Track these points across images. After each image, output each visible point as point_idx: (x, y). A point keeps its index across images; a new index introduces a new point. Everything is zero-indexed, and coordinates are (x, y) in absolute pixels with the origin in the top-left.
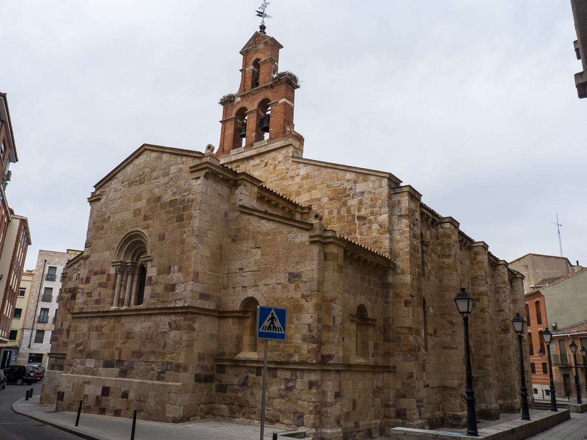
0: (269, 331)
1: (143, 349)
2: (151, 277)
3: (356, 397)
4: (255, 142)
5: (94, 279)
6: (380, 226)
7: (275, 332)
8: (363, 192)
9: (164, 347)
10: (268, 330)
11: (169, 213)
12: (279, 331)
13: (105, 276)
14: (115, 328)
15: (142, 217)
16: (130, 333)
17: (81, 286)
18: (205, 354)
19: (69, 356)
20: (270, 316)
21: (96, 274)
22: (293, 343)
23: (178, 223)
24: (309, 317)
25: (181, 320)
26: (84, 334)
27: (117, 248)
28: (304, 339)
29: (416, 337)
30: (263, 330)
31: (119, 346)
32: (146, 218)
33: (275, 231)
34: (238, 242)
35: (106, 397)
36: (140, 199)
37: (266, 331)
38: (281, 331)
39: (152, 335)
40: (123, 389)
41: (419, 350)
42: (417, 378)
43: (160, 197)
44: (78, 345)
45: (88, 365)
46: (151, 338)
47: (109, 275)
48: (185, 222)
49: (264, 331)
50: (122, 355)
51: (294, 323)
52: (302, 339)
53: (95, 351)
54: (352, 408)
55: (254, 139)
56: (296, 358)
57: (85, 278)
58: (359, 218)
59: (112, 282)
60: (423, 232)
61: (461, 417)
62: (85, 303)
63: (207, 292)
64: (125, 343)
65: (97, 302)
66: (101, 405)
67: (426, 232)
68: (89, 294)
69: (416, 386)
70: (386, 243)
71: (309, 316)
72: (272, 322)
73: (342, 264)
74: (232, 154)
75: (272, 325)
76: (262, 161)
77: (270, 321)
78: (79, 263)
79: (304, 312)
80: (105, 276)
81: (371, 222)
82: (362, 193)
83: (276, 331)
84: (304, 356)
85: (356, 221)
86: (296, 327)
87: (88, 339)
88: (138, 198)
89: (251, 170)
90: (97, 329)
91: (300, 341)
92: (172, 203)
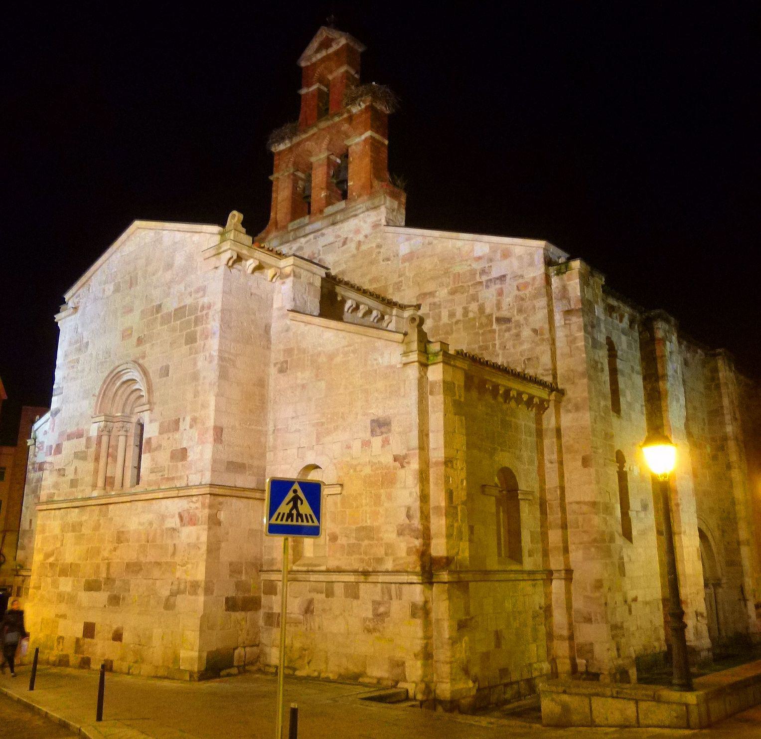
0: (289, 522)
1: (142, 559)
2: (150, 438)
3: (502, 627)
4: (326, 207)
5: (69, 447)
6: (535, 331)
7: (300, 523)
8: (504, 276)
9: (174, 554)
10: (287, 520)
11: (174, 330)
12: (308, 521)
13: (83, 440)
14: (100, 525)
15: (134, 339)
16: (123, 532)
17: (49, 459)
18: (241, 563)
19: (35, 574)
20: (291, 495)
21: (70, 437)
22: (382, 539)
23: (189, 346)
24: (408, 495)
25: (197, 508)
26: (55, 537)
27: (99, 394)
28: (400, 533)
29: (605, 519)
30: (277, 520)
31: (106, 554)
32: (140, 341)
33: (346, 349)
34: (288, 371)
35: (89, 640)
36: (131, 310)
37: (284, 522)
38: (313, 522)
39: (155, 534)
40: (115, 627)
41: (612, 540)
42: (609, 589)
43: (160, 306)
44: (47, 556)
45: (62, 588)
46: (154, 541)
47: (89, 439)
48: (200, 342)
49: (279, 522)
50: (112, 570)
51: (383, 505)
52: (398, 531)
53: (71, 564)
54: (493, 644)
55: (324, 202)
56: (389, 565)
57: (54, 446)
58: (499, 320)
59: (93, 449)
60: (614, 339)
61: (697, 649)
62: (56, 485)
63: (239, 460)
64: (115, 549)
65: (74, 483)
66: (82, 653)
67: (620, 337)
68: (61, 472)
69: (609, 601)
70: (546, 359)
71: (406, 493)
72: (295, 506)
73: (462, 399)
74: (290, 228)
75: (294, 512)
76: (339, 236)
77: (291, 504)
78: (555, 452)
79: (398, 485)
80: (83, 440)
81: (518, 325)
82: (502, 278)
83: (302, 521)
84: (401, 562)
85: (495, 326)
86: (387, 510)
87: (62, 545)
88: (129, 310)
89: (321, 253)
90: (76, 527)
91: (394, 536)
92: (180, 312)
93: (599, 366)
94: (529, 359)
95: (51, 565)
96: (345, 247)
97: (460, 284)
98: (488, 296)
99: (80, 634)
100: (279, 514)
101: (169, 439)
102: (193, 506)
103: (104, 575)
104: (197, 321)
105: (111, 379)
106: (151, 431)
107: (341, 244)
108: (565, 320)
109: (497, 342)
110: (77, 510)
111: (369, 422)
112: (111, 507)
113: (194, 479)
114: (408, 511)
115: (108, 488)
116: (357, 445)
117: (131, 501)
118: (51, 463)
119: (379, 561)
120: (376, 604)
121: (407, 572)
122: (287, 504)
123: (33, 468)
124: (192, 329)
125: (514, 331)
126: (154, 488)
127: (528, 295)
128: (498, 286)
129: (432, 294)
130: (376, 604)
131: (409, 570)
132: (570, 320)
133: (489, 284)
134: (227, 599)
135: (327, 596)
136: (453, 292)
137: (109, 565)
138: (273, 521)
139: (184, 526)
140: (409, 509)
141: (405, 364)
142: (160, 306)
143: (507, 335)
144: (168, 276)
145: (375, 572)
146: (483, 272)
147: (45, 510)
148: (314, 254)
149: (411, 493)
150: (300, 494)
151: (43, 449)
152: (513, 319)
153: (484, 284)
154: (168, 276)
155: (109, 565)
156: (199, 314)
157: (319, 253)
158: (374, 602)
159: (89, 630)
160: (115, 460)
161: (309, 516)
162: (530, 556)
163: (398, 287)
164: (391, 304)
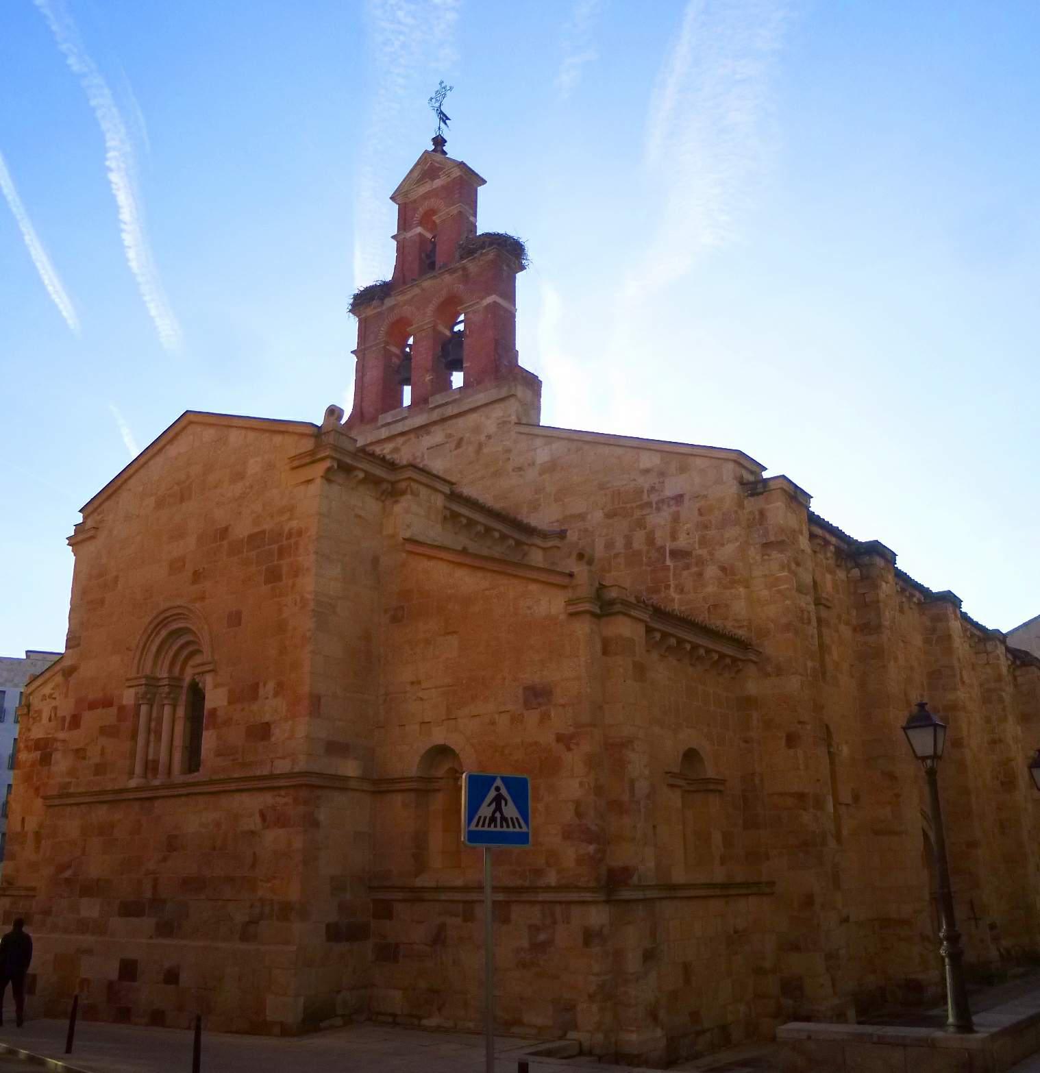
0: (492, 829)
2: (215, 710)
7: (505, 829)
8: (681, 496)
9: (253, 866)
10: (489, 826)
12: (514, 827)
20: (492, 794)
21: (92, 706)
23: (270, 586)
24: (577, 785)
25: (286, 804)
27: (137, 647)
28: (567, 835)
30: (477, 825)
37: (486, 828)
38: (520, 827)
43: (226, 529)
45: (84, 913)
47: (121, 709)
49: (480, 828)
56: (552, 878)
58: (675, 554)
62: (72, 772)
64: (165, 859)
65: (100, 769)
68: (80, 753)
71: (575, 783)
72: (498, 808)
75: (498, 815)
77: (494, 805)
81: (701, 562)
82: (679, 498)
83: (508, 826)
85: (668, 562)
89: (426, 457)
92: (255, 539)
93: (805, 616)
94: (715, 606)
95: (67, 880)
96: (460, 451)
97: (621, 505)
98: (659, 520)
99: (114, 976)
100: (480, 817)
101: (243, 710)
102: (282, 800)
103: (148, 895)
104: (281, 552)
105: (156, 627)
106: (215, 698)
107: (453, 446)
108: (763, 555)
109: (672, 583)
110: (105, 807)
111: (521, 691)
112: (157, 803)
113: (283, 766)
114: (576, 808)
115: (149, 775)
116: (503, 721)
117: (188, 795)
118: (64, 741)
119: (539, 872)
120: (534, 929)
121: (576, 887)
122: (489, 805)
123: (26, 747)
124: (276, 562)
125: (694, 569)
126: (222, 777)
127: (713, 522)
128: (674, 509)
129: (582, 517)
130: (534, 929)
131: (580, 884)
132: (769, 555)
133: (660, 505)
134: (328, 926)
135: (466, 920)
136: (609, 516)
137: (156, 880)
138: (473, 827)
139: (268, 827)
140: (578, 804)
141: (571, 615)
142: (226, 529)
143: (685, 573)
144: (238, 488)
145: (534, 889)
146: (652, 489)
147: (56, 806)
148: (415, 458)
149: (581, 784)
150: (504, 791)
151: (40, 720)
152: (694, 552)
153: (654, 506)
154: (238, 488)
155: (156, 880)
156: (285, 542)
157: (423, 456)
158: (530, 927)
159: (129, 970)
160: (158, 734)
161: (515, 820)
162: (722, 864)
163: (535, 506)
164: (530, 531)
